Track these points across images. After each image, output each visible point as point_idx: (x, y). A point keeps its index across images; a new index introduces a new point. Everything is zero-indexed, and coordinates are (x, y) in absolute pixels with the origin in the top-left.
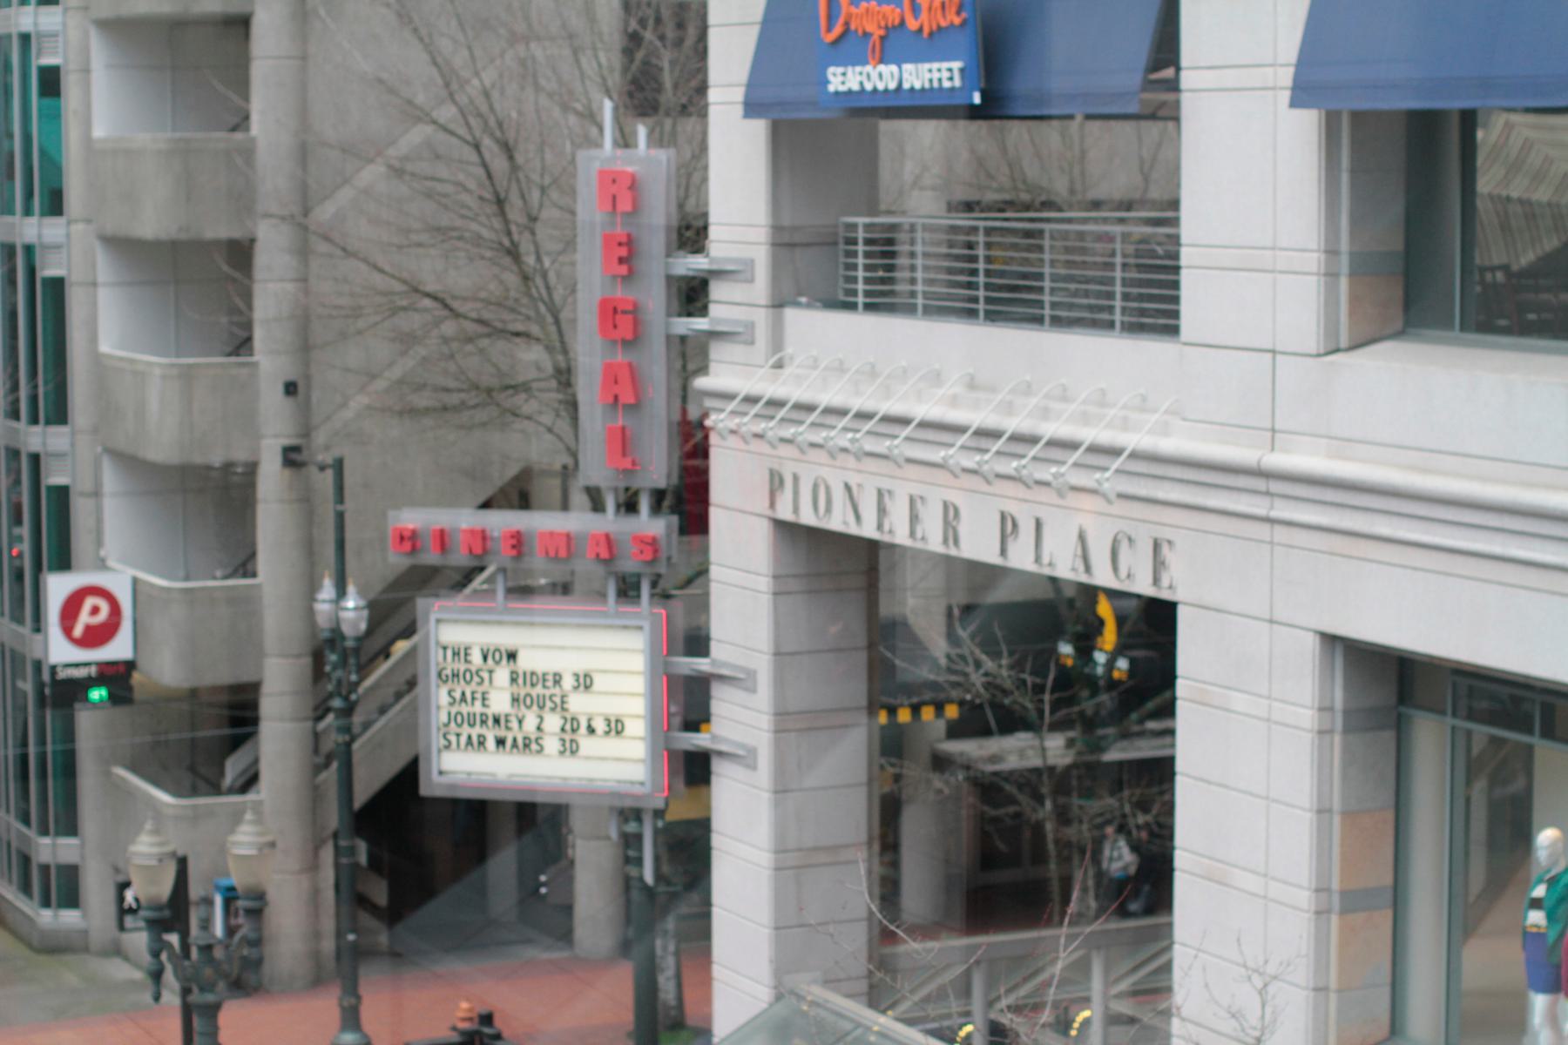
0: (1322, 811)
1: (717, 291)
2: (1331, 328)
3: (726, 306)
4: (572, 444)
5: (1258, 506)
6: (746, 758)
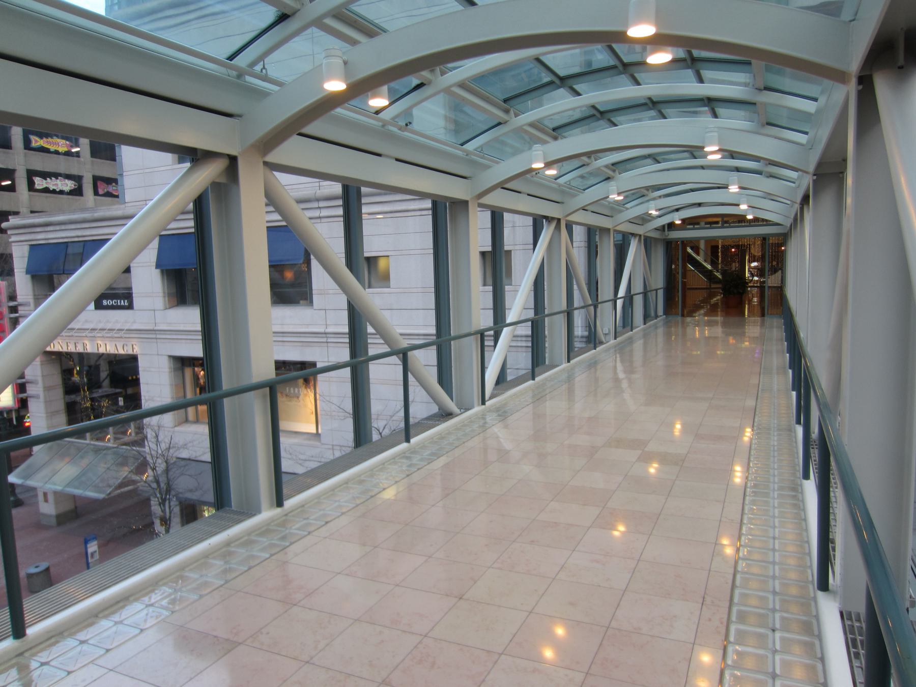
0: (171, 385)
1: (20, 308)
2: (165, 305)
3: (22, 311)
4: (125, 622)
5: (154, 336)
6: (37, 397)
